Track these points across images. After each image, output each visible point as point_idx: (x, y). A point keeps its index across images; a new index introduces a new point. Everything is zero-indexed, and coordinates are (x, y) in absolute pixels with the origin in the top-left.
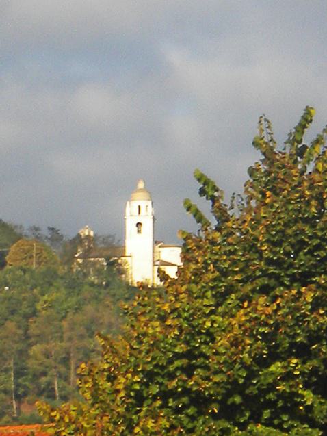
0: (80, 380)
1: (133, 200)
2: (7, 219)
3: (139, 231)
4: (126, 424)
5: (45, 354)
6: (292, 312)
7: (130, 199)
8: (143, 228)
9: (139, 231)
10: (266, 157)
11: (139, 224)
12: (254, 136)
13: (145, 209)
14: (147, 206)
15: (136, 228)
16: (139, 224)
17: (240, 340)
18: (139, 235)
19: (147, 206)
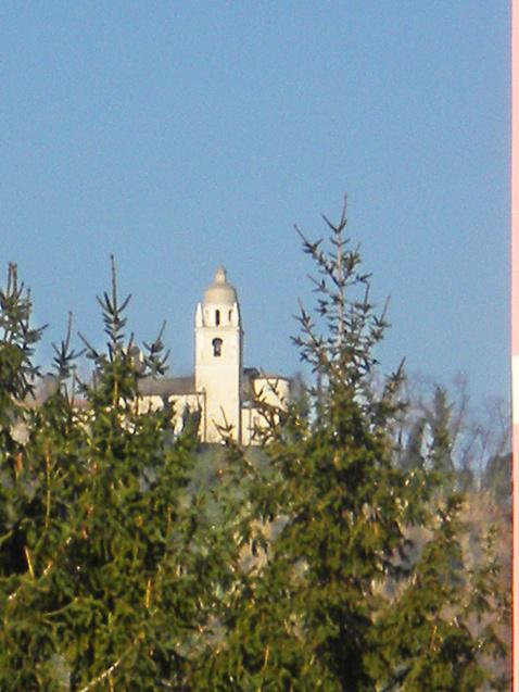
0: (371, 463)
1: (209, 302)
2: (514, 2)
3: (217, 353)
4: (6, 392)
5: (351, 428)
6: (6, 386)
7: (202, 301)
8: (223, 348)
9: (217, 353)
10: (226, 280)
11: (217, 342)
12: (101, 321)
13: (227, 317)
14: (230, 313)
15: (213, 348)
16: (217, 342)
17: (107, 421)
18: (218, 358)
19: (230, 313)
